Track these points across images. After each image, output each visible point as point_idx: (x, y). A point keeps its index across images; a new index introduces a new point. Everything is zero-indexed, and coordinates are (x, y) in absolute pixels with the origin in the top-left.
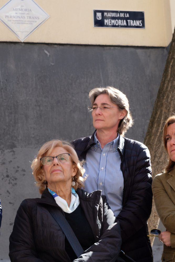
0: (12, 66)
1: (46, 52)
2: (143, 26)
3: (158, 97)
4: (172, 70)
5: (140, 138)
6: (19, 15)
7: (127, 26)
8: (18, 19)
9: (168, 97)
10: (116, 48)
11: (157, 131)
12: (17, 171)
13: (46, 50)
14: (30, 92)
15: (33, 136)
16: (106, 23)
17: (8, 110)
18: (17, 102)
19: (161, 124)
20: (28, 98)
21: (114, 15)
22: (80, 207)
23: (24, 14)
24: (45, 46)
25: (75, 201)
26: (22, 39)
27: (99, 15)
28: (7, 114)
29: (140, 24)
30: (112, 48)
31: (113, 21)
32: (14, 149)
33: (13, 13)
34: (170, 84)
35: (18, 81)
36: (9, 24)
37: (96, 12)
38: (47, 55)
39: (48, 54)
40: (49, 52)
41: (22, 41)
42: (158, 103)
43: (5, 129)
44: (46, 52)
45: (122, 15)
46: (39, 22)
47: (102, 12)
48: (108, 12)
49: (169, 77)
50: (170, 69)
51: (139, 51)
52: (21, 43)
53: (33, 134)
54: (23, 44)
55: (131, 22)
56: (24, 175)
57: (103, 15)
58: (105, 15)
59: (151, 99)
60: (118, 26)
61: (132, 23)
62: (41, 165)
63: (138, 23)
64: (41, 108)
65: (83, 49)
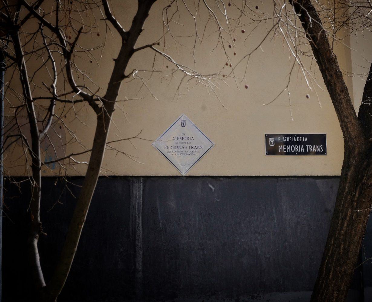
1: (211, 186)
2: (324, 152)
6: (179, 145)
7: (306, 153)
8: (178, 150)
10: (292, 178)
13: (211, 184)
16: (281, 150)
20: (190, 240)
26: (184, 173)
30: (287, 179)
37: (268, 137)
38: (212, 189)
40: (213, 186)
44: (211, 186)
45: (299, 139)
50: (325, 266)
51: (318, 181)
52: (182, 176)
60: (294, 153)
63: (318, 148)
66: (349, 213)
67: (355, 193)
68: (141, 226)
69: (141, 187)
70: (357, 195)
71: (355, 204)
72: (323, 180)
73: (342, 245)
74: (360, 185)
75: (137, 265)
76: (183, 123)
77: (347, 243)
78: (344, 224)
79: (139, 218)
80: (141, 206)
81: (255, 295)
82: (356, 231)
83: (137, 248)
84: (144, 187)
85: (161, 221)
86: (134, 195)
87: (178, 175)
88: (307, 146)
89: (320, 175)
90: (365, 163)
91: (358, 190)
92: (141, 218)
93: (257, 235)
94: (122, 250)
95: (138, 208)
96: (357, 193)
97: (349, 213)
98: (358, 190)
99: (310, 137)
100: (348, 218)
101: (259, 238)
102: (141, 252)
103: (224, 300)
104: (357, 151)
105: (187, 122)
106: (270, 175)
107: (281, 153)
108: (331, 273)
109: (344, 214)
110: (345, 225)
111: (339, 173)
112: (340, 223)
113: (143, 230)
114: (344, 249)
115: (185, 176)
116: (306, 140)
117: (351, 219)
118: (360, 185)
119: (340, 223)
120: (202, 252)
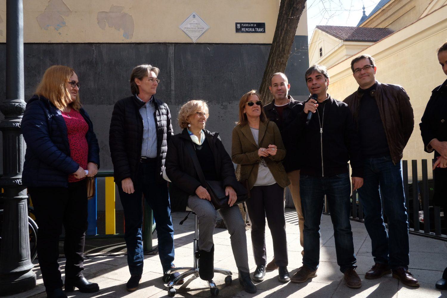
1: (208, 48)
2: (264, 32)
3: (264, 76)
4: (272, 60)
6: (192, 27)
7: (255, 32)
8: (192, 29)
10: (249, 45)
13: (208, 47)
14: (199, 72)
15: (202, 97)
16: (243, 30)
17: (187, 82)
18: (192, 78)
20: (198, 75)
21: (247, 25)
22: (206, 139)
24: (208, 45)
25: (203, 136)
26: (194, 41)
27: (239, 25)
28: (187, 85)
29: (262, 30)
30: (246, 45)
31: (247, 29)
33: (189, 26)
34: (270, 68)
35: (193, 66)
36: (187, 32)
37: (237, 24)
38: (209, 50)
39: (210, 49)
42: (263, 79)
44: (208, 48)
45: (252, 25)
46: (204, 30)
47: (241, 24)
48: (244, 23)
49: (270, 64)
50: (271, 59)
51: (262, 46)
52: (194, 43)
54: (195, 44)
55: (257, 29)
58: (75, 74)
60: (250, 32)
61: (258, 30)
62: (318, 94)
63: (261, 30)
65: (229, 46)
66: (285, 26)
67: (289, 14)
68: (173, 68)
69: (173, 49)
71: (289, 20)
72: (264, 46)
73: (281, 46)
74: (292, 8)
75: (172, 87)
77: (244, 218)
79: (172, 64)
80: (173, 58)
81: (231, 102)
82: (289, 38)
83: (171, 79)
86: (170, 53)
87: (192, 42)
88: (256, 29)
89: (262, 43)
91: (291, 11)
92: (173, 64)
93: (231, 72)
95: (172, 59)
96: (290, 13)
97: (285, 26)
98: (291, 11)
99: (257, 24)
101: (233, 74)
102: (174, 81)
103: (215, 105)
105: (196, 15)
106: (238, 43)
107: (243, 32)
108: (274, 63)
109: (282, 27)
110: (283, 33)
111: (271, 42)
112: (280, 33)
113: (175, 70)
114: (282, 48)
115: (195, 43)
116: (255, 25)
117: (287, 29)
118: (292, 8)
119: (280, 33)
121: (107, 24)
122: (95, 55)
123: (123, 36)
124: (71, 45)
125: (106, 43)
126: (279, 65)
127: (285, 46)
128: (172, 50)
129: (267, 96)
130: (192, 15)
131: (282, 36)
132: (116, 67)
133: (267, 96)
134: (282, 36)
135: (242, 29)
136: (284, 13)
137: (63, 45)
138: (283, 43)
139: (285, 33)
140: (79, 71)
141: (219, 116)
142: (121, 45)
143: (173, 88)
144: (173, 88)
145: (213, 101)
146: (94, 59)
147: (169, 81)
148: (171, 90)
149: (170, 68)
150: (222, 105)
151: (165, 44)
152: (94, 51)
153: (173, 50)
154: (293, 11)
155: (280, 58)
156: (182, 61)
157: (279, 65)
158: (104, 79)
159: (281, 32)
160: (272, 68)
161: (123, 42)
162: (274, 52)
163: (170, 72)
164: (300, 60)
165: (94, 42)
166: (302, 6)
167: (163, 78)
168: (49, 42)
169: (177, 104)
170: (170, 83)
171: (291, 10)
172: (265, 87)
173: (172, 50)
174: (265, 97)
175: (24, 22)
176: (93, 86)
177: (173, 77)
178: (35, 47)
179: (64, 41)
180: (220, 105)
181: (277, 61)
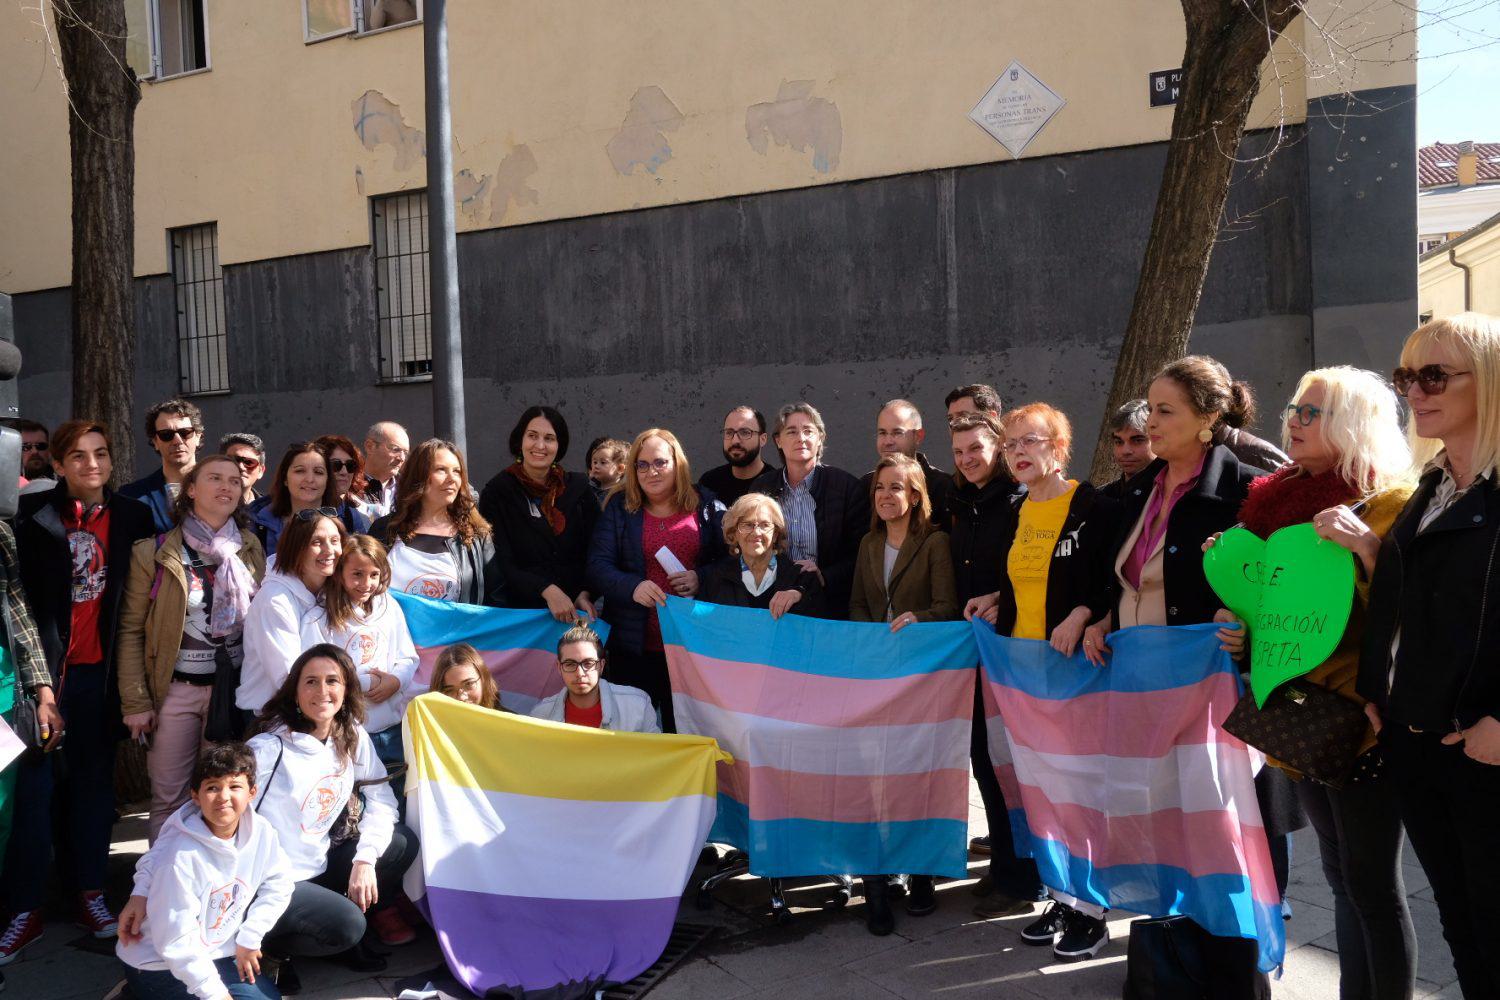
0: (1000, 206)
1: (1060, 170)
5: (1240, 312)
9: (1143, 308)
11: (1127, 368)
12: (1013, 387)
13: (1061, 167)
15: (1040, 325)
19: (1133, 358)
23: (1012, 107)
24: (1059, 159)
27: (1161, 81)
28: (993, 291)
32: (1008, 351)
34: (1148, 284)
38: (1061, 175)
39: (1064, 173)
40: (1065, 170)
41: (1016, 158)
43: (991, 318)
44: (1060, 170)
53: (1039, 322)
56: (1024, 393)
57: (1168, 80)
59: (1265, 234)
64: (1053, 274)
67: (1201, 111)
70: (1204, 115)
73: (1178, 215)
75: (950, 303)
76: (1014, 73)
78: (1181, 173)
79: (950, 231)
80: (954, 213)
83: (949, 277)
84: (957, 183)
85: (984, 233)
90: (1219, 50)
94: (927, 282)
100: (1188, 162)
102: (955, 283)
103: (1082, 346)
104: (1204, 28)
105: (1020, 72)
108: (1159, 268)
110: (1183, 176)
113: (957, 248)
114: (1182, 220)
117: (1194, 161)
120: (1047, 276)
121: (771, 137)
122: (744, 227)
123: (814, 165)
124: (685, 207)
125: (772, 192)
126: (1172, 273)
127: (1191, 213)
128: (948, 189)
129: (1138, 370)
130: (1008, 73)
131: (1182, 182)
132: (798, 257)
133: (1138, 370)
134: (1182, 182)
135: (1171, 91)
136: (1185, 109)
137: (667, 210)
138: (1183, 205)
139: (1190, 174)
140: (707, 276)
141: (1094, 383)
142: (809, 191)
143: (953, 304)
144: (953, 304)
145: (1075, 336)
146: (742, 240)
147: (942, 285)
148: (947, 311)
149: (944, 243)
150: (1103, 347)
151: (929, 174)
152: (741, 218)
153: (953, 190)
154: (1211, 101)
155: (1177, 252)
156: (980, 218)
157: (1172, 273)
158: (768, 294)
159: (1177, 172)
160: (1151, 283)
161: (814, 184)
162: (1157, 234)
163: (944, 256)
164: (1379, 179)
165: (741, 193)
166: (1243, 80)
167: (924, 275)
168: (636, 208)
169: (964, 351)
170: (946, 289)
171: (1206, 100)
172: (1133, 344)
173: (948, 189)
174: (1133, 371)
175: (460, 287)
176: (740, 316)
177: (953, 272)
178: (606, 222)
179: (669, 201)
180: (1099, 347)
181: (1166, 263)
